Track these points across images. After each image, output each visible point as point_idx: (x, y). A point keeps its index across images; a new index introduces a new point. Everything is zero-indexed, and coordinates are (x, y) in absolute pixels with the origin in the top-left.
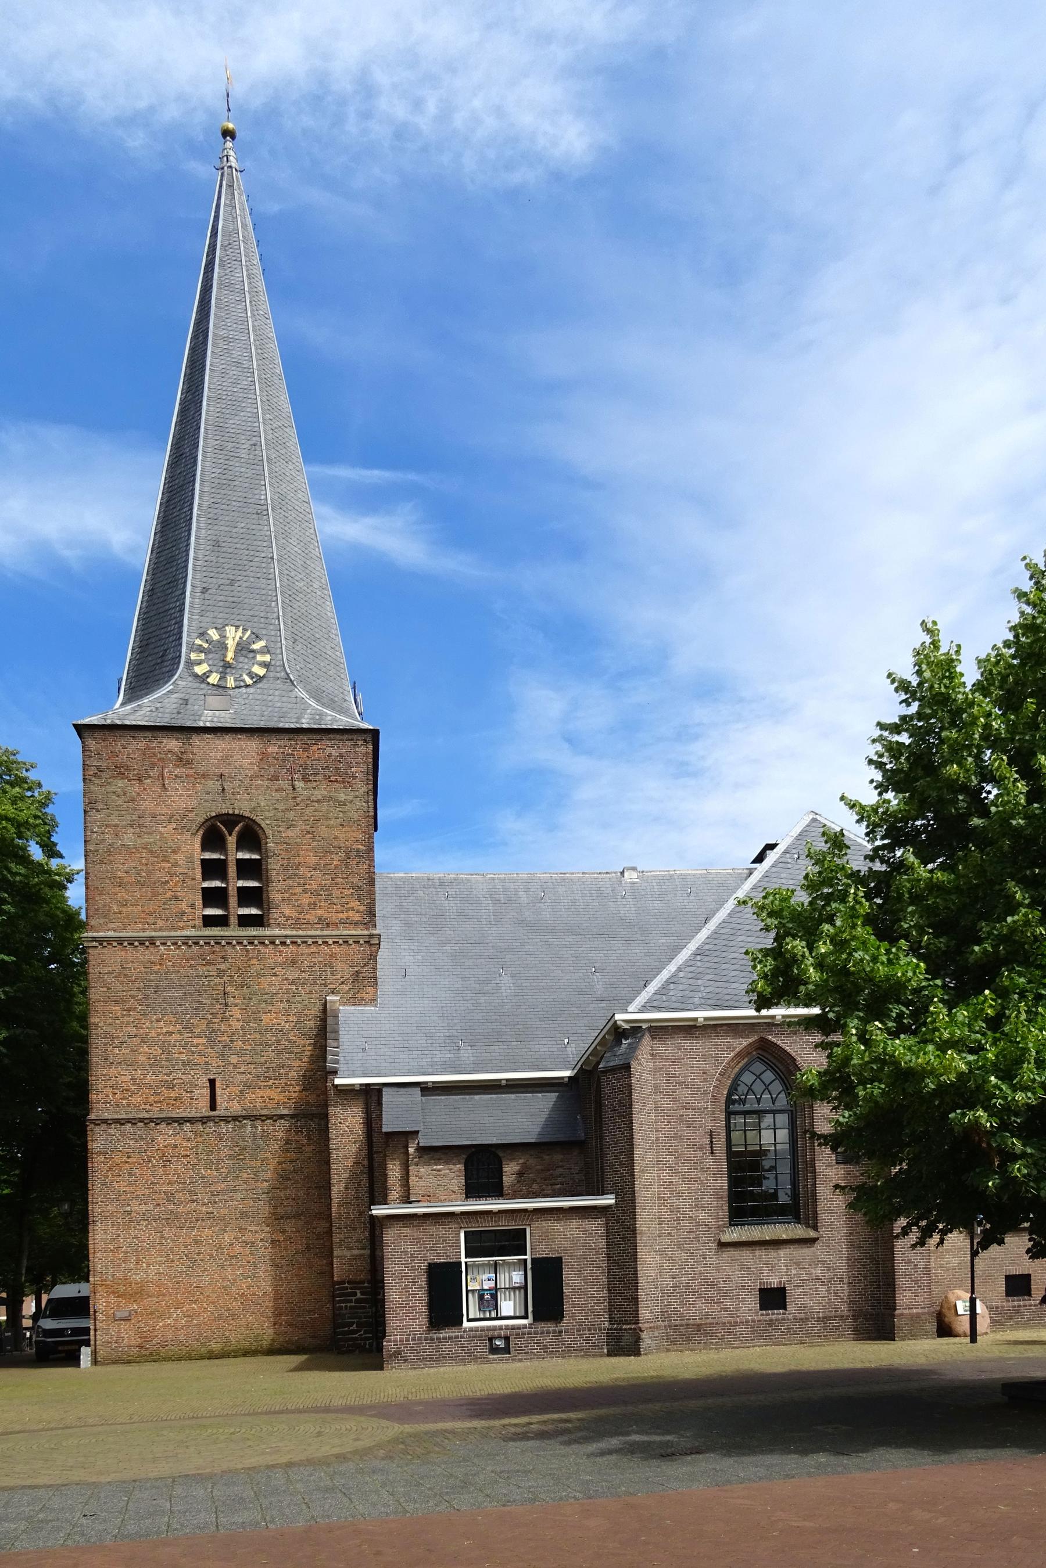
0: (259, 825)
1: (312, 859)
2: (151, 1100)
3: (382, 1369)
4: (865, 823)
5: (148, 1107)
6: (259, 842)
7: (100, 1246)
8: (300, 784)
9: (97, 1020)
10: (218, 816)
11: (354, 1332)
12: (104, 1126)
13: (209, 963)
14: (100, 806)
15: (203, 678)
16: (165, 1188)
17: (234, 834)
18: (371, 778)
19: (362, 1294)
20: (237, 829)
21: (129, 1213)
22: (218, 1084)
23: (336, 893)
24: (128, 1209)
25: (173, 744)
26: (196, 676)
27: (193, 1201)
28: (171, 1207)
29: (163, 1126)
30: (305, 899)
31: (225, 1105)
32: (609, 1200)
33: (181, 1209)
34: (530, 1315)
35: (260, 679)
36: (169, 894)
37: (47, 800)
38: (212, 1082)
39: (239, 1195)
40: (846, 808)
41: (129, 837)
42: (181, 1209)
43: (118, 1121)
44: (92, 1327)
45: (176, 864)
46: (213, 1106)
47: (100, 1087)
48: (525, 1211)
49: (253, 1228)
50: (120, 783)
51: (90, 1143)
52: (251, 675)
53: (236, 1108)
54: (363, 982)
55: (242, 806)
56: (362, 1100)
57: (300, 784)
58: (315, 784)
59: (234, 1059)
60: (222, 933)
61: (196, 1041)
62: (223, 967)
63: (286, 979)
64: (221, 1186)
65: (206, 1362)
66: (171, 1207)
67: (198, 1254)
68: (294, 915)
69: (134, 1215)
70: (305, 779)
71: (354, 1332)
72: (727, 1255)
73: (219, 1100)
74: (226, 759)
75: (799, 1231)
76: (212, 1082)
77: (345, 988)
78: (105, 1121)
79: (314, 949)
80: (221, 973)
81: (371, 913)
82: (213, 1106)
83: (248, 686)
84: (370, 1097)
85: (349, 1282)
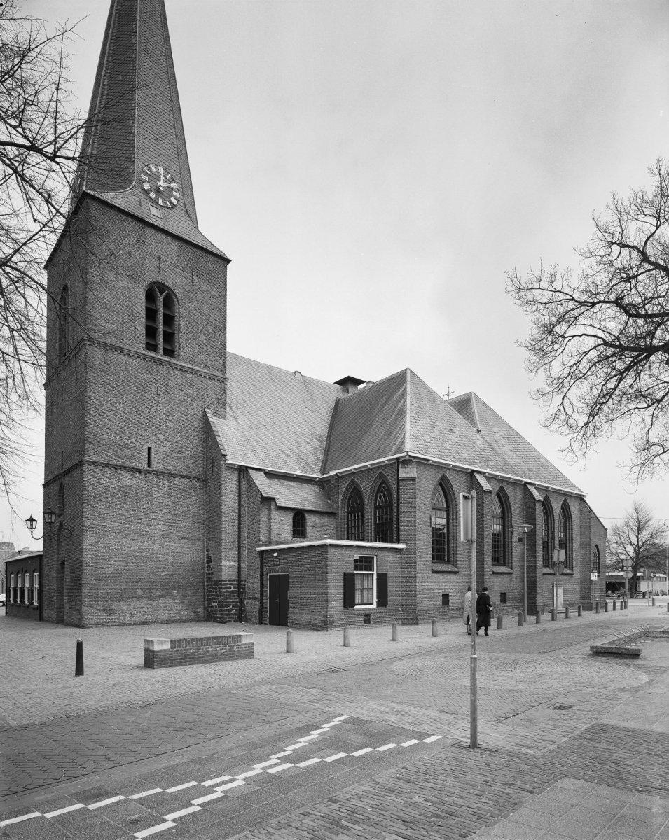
0: (176, 296)
3: (417, 624)
6: (154, 300)
8: (195, 278)
9: (90, 395)
10: (156, 283)
11: (231, 610)
15: (147, 192)
16: (125, 513)
17: (163, 296)
19: (234, 588)
20: (164, 294)
21: (105, 527)
22: (153, 451)
24: (105, 524)
26: (144, 189)
27: (139, 523)
32: (402, 546)
33: (133, 528)
35: (174, 206)
38: (149, 449)
42: (133, 528)
46: (149, 464)
48: (375, 548)
52: (171, 203)
54: (221, 403)
55: (169, 282)
56: (236, 474)
57: (195, 278)
59: (161, 437)
60: (168, 360)
62: (156, 377)
64: (152, 516)
65: (138, 627)
71: (231, 610)
72: (435, 575)
75: (451, 568)
76: (149, 449)
77: (213, 406)
81: (225, 366)
82: (149, 464)
83: (168, 208)
84: (243, 471)
85: (228, 581)
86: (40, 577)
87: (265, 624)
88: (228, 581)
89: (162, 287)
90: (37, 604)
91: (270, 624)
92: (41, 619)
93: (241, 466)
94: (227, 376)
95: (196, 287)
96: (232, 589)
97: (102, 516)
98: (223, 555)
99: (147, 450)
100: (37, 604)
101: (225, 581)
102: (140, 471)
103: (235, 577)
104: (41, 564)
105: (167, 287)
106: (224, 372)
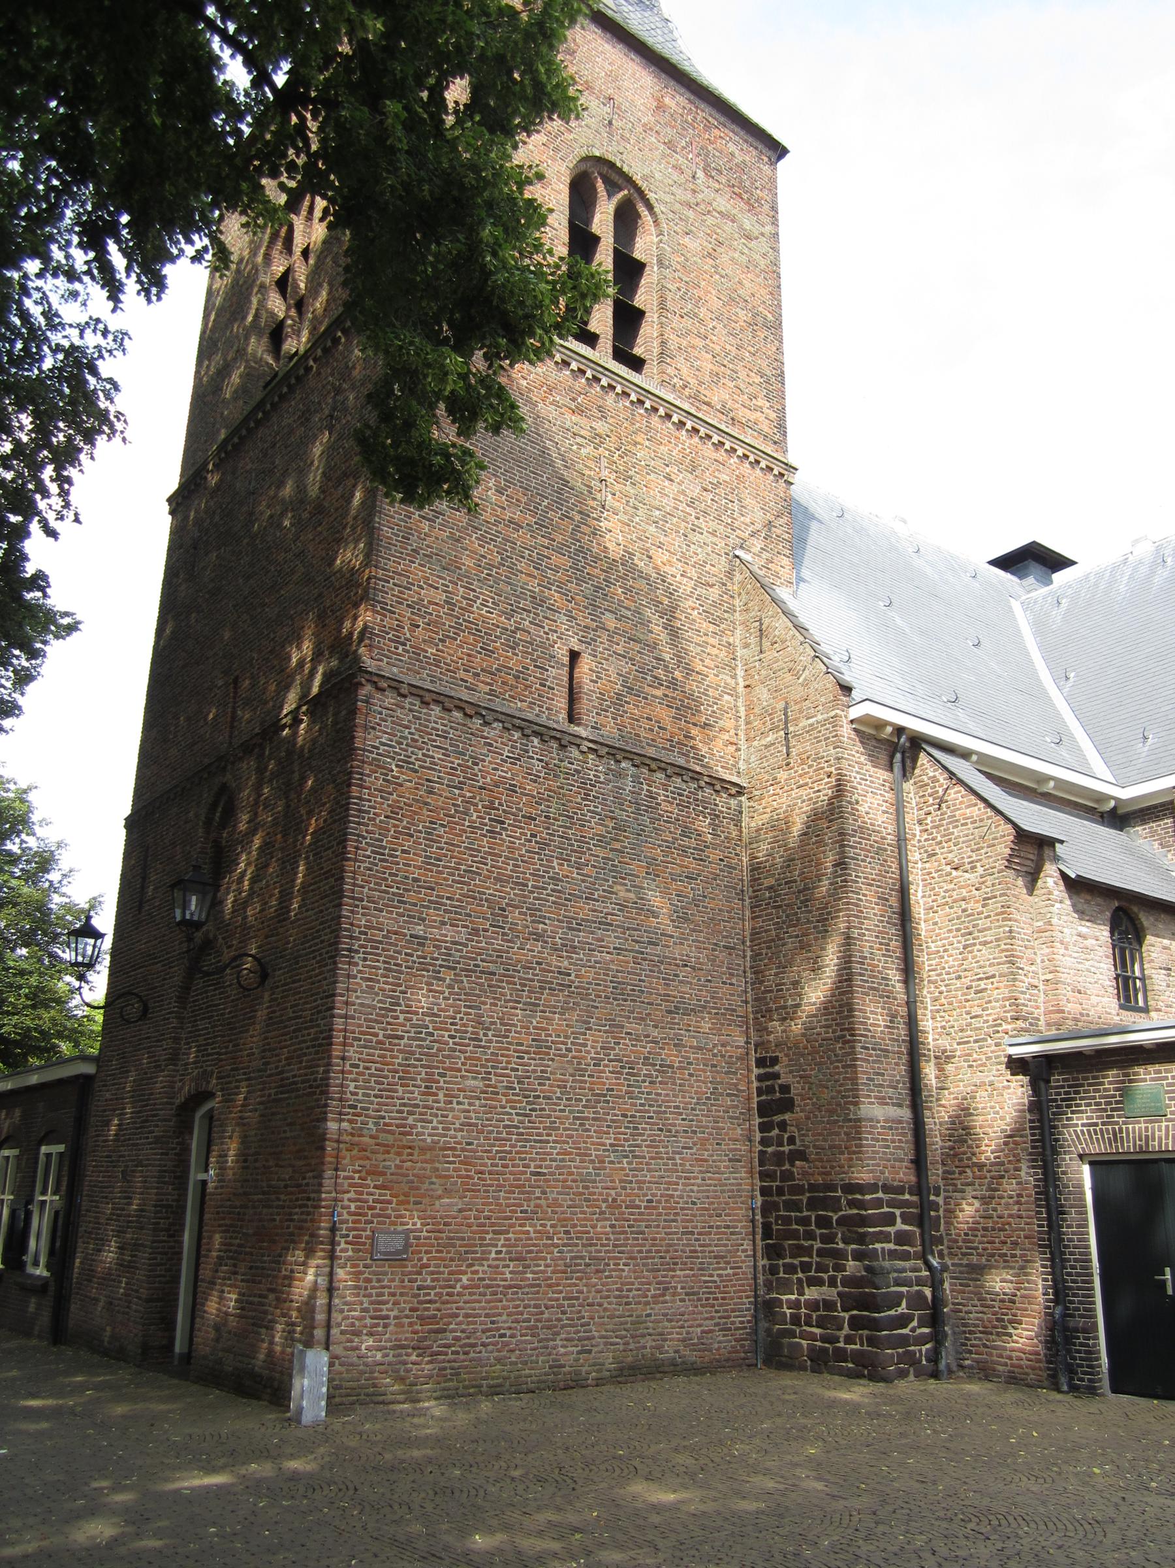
1: (716, 304)
4: (988, 1149)
5: (469, 678)
7: (358, 1024)
10: (599, 160)
12: (390, 699)
13: (579, 411)
21: (420, 940)
24: (419, 930)
27: (538, 937)
28: (498, 943)
29: (494, 732)
34: (42, 1158)
37: (531, 363)
38: (574, 656)
39: (612, 939)
43: (417, 692)
44: (896, 1275)
47: (389, 599)
51: (359, 734)
53: (610, 731)
55: (635, 167)
58: (717, 186)
59: (610, 621)
61: (556, 559)
63: (683, 492)
64: (584, 910)
66: (498, 943)
78: (395, 686)
79: (721, 455)
81: (781, 426)
82: (572, 718)
85: (887, 1189)
86: (73, 1164)
87: (1092, 1391)
88: (887, 1189)
89: (616, 177)
90: (41, 1271)
91: (765, 1363)
92: (58, 1334)
93: (900, 730)
94: (792, 459)
95: (700, 196)
96: (900, 1226)
97: (411, 897)
98: (862, 1079)
99: (566, 660)
100: (41, 1271)
101: (873, 1188)
102: (543, 733)
103: (905, 1175)
104: (81, 1124)
105: (629, 180)
106: (780, 442)
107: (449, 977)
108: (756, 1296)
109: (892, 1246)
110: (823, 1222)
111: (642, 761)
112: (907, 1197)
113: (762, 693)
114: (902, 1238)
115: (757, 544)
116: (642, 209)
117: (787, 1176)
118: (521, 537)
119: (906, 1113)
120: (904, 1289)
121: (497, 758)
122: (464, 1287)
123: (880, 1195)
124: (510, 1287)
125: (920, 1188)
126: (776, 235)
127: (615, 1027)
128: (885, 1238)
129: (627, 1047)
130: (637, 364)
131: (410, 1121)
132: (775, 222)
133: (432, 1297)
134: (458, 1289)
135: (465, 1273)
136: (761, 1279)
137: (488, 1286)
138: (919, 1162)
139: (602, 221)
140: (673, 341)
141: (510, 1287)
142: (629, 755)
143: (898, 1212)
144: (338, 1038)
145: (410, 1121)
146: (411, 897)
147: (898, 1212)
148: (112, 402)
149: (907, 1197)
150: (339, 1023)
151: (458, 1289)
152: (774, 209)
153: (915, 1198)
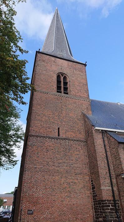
2: (45, 131)
12: (32, 137)
14: (39, 66)
18: (28, 139)
21: (36, 168)
22: (60, 129)
23: (82, 91)
25: (53, 59)
27: (54, 165)
28: (48, 167)
30: (76, 91)
31: (62, 135)
36: (51, 85)
38: (59, 128)
40: (16, 27)
41: (44, 72)
45: (53, 79)
48: (115, 132)
49: (69, 177)
50: (43, 63)
53: (64, 137)
61: (56, 117)
64: (61, 161)
66: (48, 167)
67: (55, 186)
68: (74, 93)
69: (37, 169)
70: (75, 70)
73: (60, 133)
74: (62, 64)
76: (59, 128)
78: (33, 136)
80: (61, 103)
82: (59, 136)
88: (108, 201)
89: (62, 74)
97: (34, 162)
98: (101, 183)
101: (105, 201)
103: (111, 198)
107: (40, 172)
108: (94, 220)
109: (110, 211)
110: (100, 206)
111: (69, 139)
112: (112, 202)
113: (86, 128)
114: (111, 209)
115: (86, 110)
116: (67, 76)
117: (96, 199)
118: (51, 116)
119: (111, 188)
120: (112, 219)
121: (49, 143)
122: (42, 219)
123: (106, 202)
124: (49, 218)
125: (114, 200)
126: (86, 75)
127: (66, 177)
128: (108, 209)
129: (68, 181)
130: (67, 94)
131: (34, 193)
132: (86, 73)
133: (36, 220)
134: (41, 219)
135: (42, 216)
136: (95, 217)
137: (46, 218)
138: (113, 196)
139: (62, 78)
140: (71, 90)
141: (49, 218)
142: (67, 139)
143: (110, 205)
144: (23, 183)
145: (34, 193)
146: (34, 162)
147: (110, 205)
148: (84, 116)
149: (112, 202)
150: (23, 181)
151: (41, 219)
152: (85, 71)
153: (113, 202)
